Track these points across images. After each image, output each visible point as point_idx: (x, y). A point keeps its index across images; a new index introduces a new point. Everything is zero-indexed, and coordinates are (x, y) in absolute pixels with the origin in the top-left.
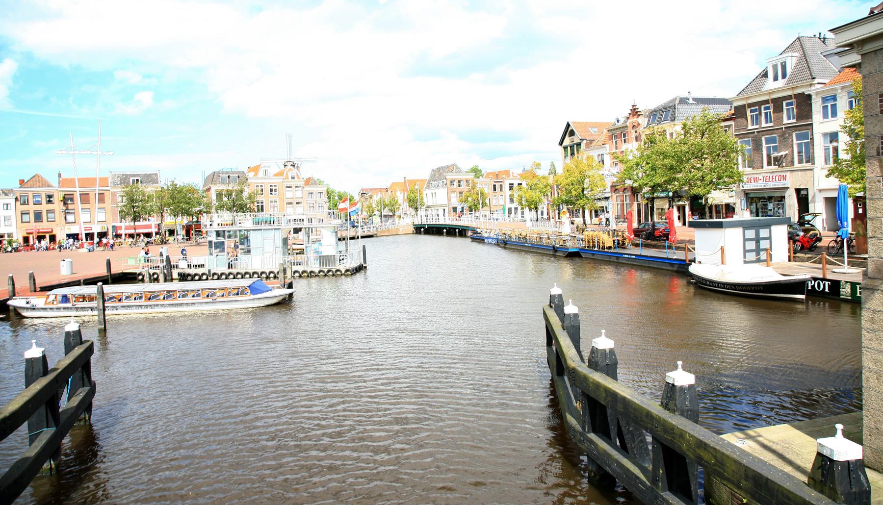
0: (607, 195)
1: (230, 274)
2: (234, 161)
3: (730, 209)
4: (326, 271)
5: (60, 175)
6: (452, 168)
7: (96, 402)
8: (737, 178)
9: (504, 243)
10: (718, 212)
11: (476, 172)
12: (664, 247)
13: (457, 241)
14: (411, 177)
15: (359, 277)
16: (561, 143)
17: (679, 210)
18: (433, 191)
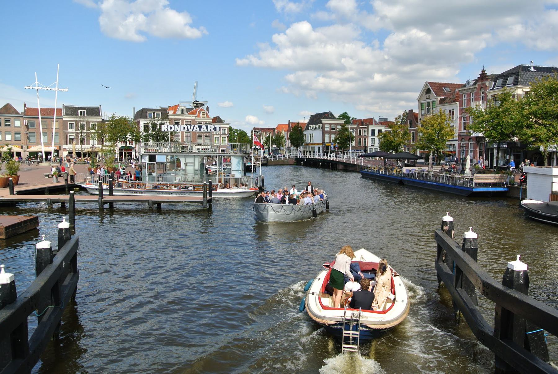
5: (25, 105)
6: (329, 115)
7: (81, 263)
11: (344, 116)
14: (294, 120)
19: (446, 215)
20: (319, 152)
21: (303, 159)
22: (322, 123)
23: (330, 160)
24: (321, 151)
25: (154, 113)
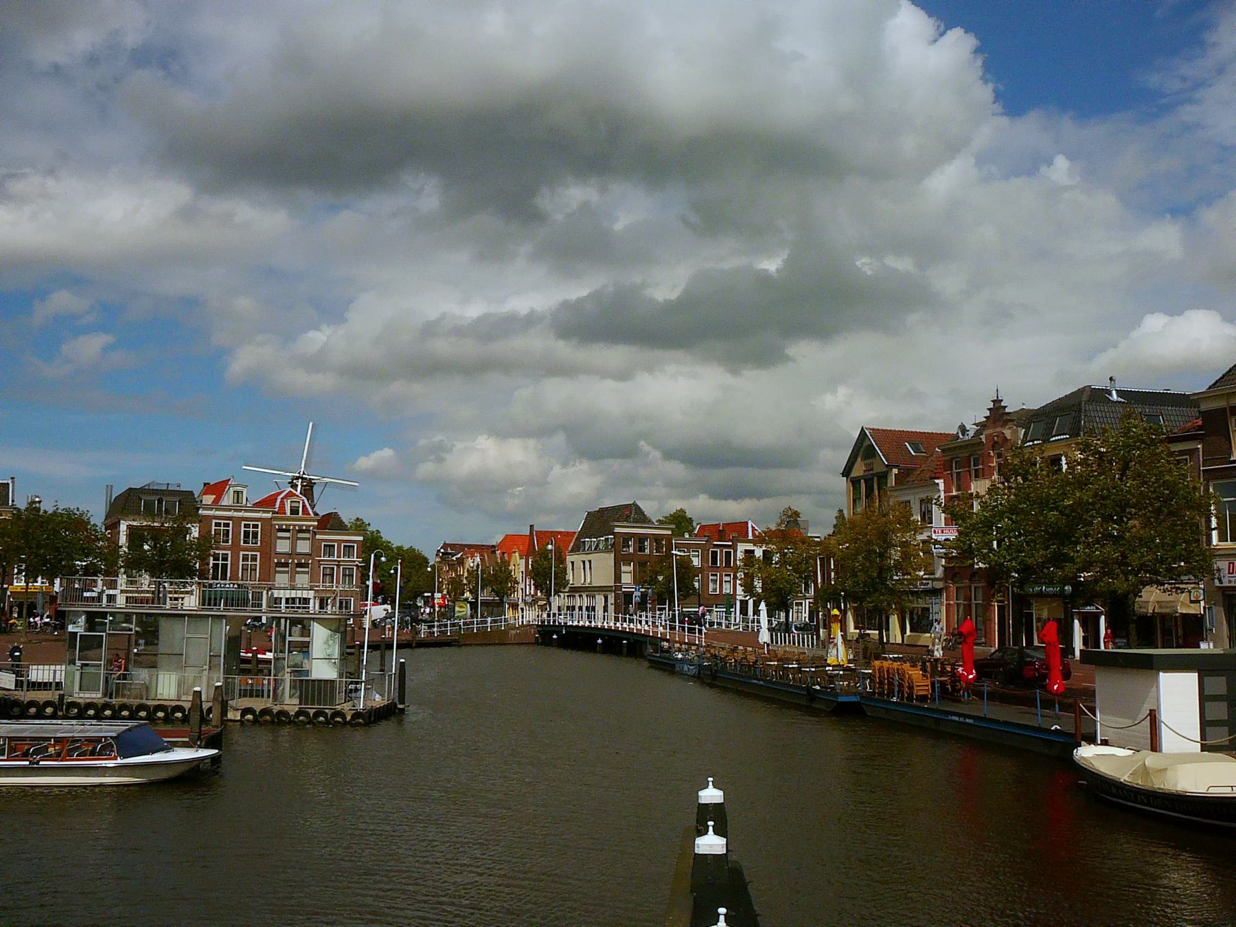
0: (939, 585)
1: (106, 706)
2: (180, 470)
3: (1193, 629)
4: (312, 712)
6: (632, 513)
8: (1202, 564)
9: (715, 675)
10: (1167, 633)
12: (1031, 703)
13: (447, 650)
15: (385, 729)
16: (846, 473)
17: (1084, 625)
18: (586, 558)
19: (706, 833)
20: (605, 609)
21: (557, 628)
22: (613, 533)
23: (624, 632)
24: (611, 608)
25: (160, 502)
